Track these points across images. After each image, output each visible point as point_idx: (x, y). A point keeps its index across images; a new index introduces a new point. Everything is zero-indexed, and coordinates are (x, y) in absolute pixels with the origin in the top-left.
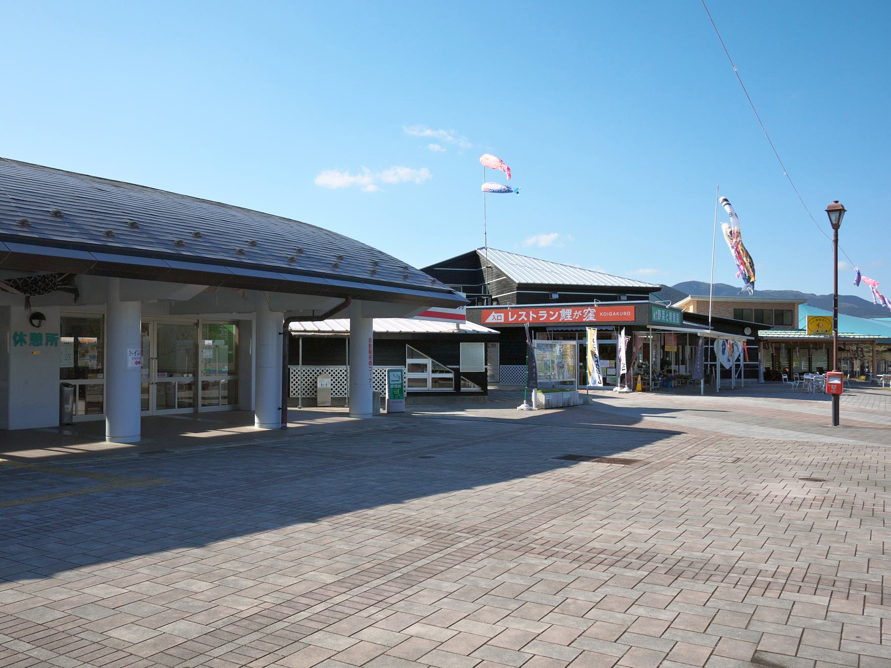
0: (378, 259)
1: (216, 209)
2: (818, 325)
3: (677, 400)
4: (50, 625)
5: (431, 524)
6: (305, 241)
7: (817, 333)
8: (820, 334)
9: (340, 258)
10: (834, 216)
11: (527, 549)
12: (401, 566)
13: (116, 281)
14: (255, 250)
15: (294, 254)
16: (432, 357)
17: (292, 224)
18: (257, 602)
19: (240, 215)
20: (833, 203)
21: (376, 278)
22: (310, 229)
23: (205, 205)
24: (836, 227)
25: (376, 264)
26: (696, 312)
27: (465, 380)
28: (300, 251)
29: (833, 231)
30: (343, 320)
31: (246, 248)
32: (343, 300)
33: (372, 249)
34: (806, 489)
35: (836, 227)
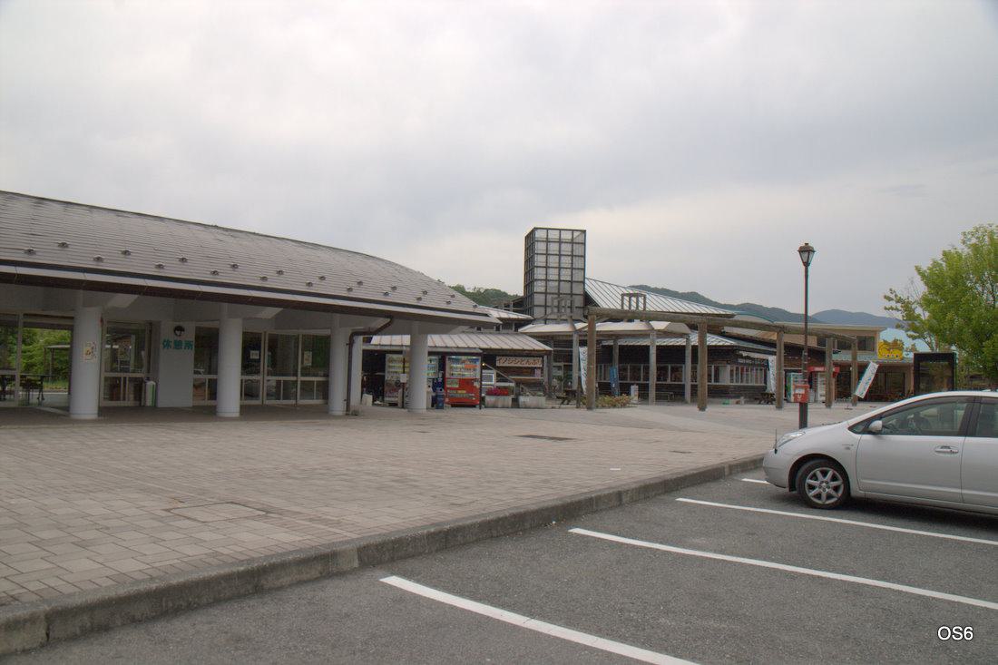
24: (806, 264)
29: (804, 267)
35: (806, 264)
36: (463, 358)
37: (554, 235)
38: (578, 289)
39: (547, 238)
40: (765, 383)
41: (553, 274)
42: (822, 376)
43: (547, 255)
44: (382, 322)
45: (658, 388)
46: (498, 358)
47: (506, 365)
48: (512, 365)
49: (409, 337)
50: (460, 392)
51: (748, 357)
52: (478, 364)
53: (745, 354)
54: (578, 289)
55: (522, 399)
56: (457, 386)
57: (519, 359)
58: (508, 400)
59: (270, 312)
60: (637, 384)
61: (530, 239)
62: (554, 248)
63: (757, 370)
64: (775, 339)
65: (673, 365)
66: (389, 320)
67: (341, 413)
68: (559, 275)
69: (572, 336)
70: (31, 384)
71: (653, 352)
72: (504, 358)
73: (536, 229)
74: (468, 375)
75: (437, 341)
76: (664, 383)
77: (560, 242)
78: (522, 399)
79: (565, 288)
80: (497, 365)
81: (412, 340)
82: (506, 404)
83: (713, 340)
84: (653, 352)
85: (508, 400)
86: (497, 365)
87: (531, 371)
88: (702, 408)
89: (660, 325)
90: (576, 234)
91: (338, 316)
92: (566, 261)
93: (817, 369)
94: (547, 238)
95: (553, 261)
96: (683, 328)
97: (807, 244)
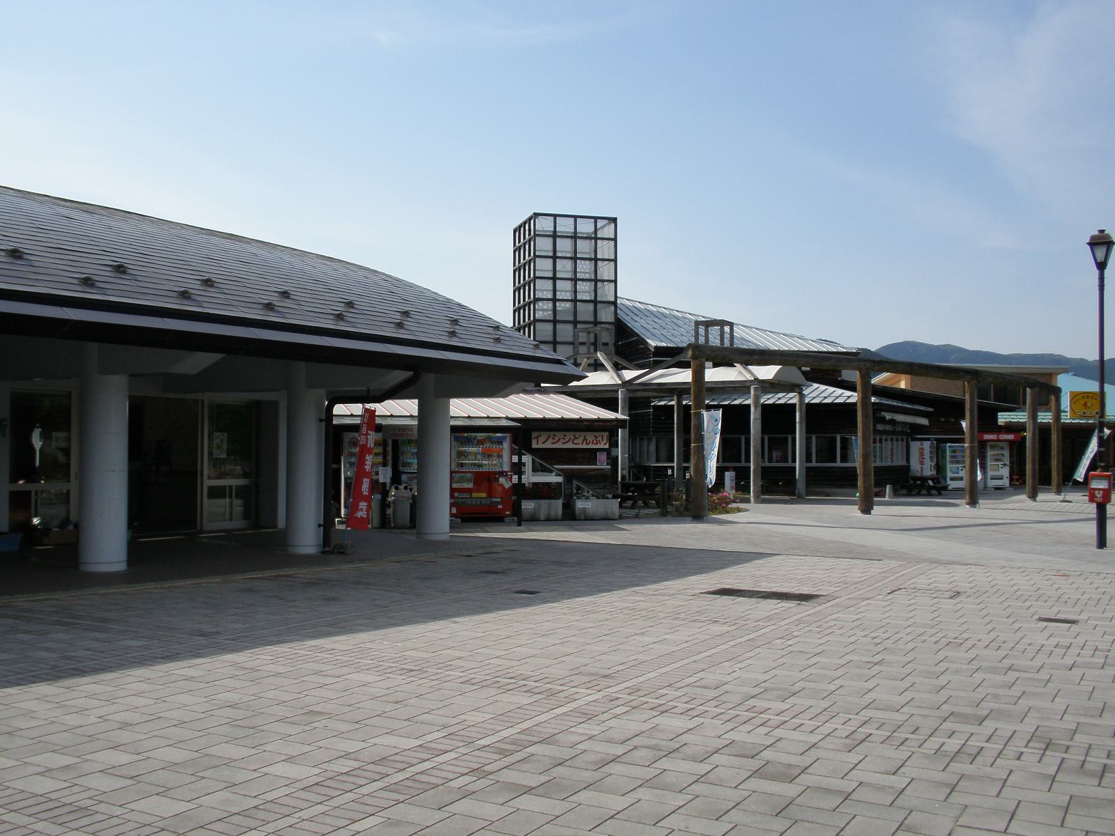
0: (408, 301)
1: (227, 244)
2: (1085, 405)
3: (754, 427)
4: (53, 796)
5: (538, 678)
6: (357, 291)
7: (1082, 417)
8: (1088, 417)
9: (406, 314)
10: (1101, 253)
11: (665, 708)
12: (500, 728)
13: (93, 348)
14: (288, 303)
15: (341, 308)
16: (532, 455)
17: (336, 265)
18: (317, 771)
19: (263, 253)
20: (1097, 233)
21: (454, 342)
22: (361, 273)
23: (215, 240)
24: (1101, 266)
25: (455, 322)
26: (909, 388)
27: (650, 441)
28: (350, 304)
29: (1097, 272)
30: (360, 404)
31: (276, 300)
32: (409, 374)
33: (449, 301)
34: (1047, 633)
35: (1101, 266)
36: (480, 435)
37: (565, 226)
38: (606, 315)
39: (555, 231)
40: (908, 460)
41: (564, 290)
42: (993, 447)
43: (575, 259)
44: (400, 376)
45: (765, 473)
46: (534, 434)
47: (549, 445)
48: (559, 446)
49: (707, 378)
50: (474, 495)
51: (892, 422)
52: (506, 445)
53: (888, 416)
54: (606, 315)
55: (580, 504)
56: (470, 485)
57: (570, 435)
58: (557, 506)
59: (198, 362)
60: (734, 469)
61: (525, 235)
62: (564, 246)
63: (892, 440)
64: (873, 398)
65: (771, 436)
66: (409, 374)
67: (311, 550)
68: (575, 292)
69: (617, 391)
70: (633, 458)
71: (754, 415)
72: (544, 436)
73: (536, 215)
74: (488, 465)
75: (462, 408)
76: (948, 459)
77: (575, 237)
78: (580, 504)
79: (585, 312)
80: (534, 445)
81: (421, 407)
82: (553, 514)
83: (820, 393)
84: (754, 415)
85: (557, 506)
86: (534, 445)
87: (590, 455)
88: (1033, 496)
89: (767, 372)
90: (600, 223)
91: (301, 367)
92: (585, 268)
93: (987, 437)
94: (555, 231)
95: (564, 267)
96: (795, 375)
97: (1102, 231)
